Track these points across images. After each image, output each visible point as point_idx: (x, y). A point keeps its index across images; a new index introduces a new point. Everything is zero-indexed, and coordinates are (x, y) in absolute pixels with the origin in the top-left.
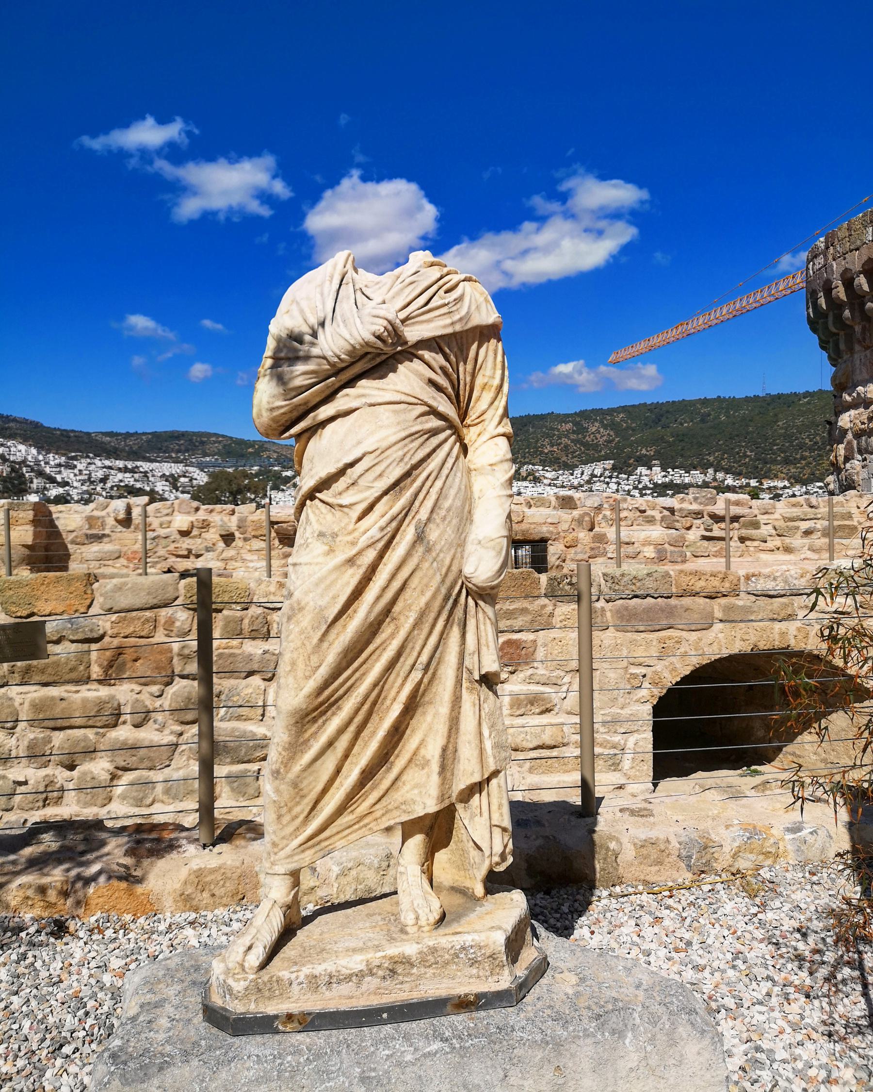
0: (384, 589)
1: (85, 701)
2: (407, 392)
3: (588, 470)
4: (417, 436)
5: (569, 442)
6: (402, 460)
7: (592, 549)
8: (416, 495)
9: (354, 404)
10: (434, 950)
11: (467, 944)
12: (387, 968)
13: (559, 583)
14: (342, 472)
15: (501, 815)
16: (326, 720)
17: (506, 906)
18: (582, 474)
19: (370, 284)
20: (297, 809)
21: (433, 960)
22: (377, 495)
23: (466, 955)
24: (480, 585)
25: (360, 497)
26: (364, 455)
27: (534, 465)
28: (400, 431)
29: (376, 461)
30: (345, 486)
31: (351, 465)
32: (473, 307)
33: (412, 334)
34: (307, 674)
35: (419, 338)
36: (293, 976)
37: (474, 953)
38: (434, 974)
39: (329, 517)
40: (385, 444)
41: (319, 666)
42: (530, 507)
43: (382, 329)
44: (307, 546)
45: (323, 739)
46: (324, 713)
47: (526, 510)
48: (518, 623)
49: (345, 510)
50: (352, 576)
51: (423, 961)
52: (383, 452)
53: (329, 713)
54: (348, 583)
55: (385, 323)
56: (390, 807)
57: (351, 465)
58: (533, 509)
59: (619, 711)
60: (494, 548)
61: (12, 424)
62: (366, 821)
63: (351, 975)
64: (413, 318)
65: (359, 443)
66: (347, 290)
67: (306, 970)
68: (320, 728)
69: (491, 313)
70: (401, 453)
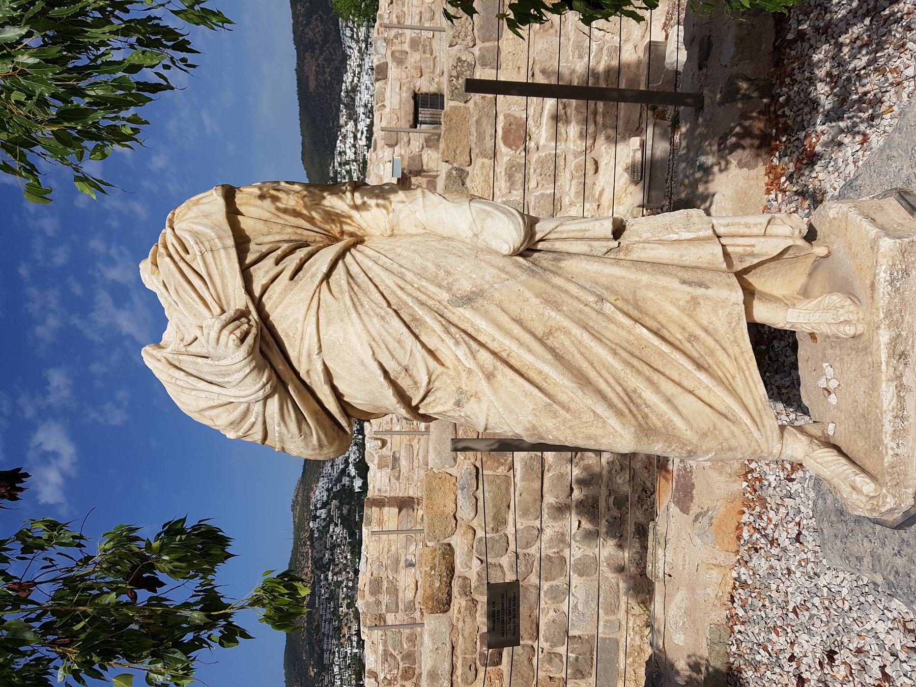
0: (521, 344)
1: (522, 480)
2: (306, 308)
3: (348, 42)
4: (355, 300)
5: (322, 57)
6: (383, 318)
7: (424, 52)
8: (422, 303)
9: (320, 367)
10: (889, 314)
11: (888, 278)
12: (898, 361)
13: (456, 88)
14: (393, 384)
15: (755, 225)
16: (645, 404)
17: (843, 226)
18: (350, 47)
19: (179, 336)
20: (726, 433)
21: (898, 315)
22: (420, 347)
23: (898, 280)
24: (522, 239)
25: (421, 367)
26: (376, 360)
27: (341, 91)
28: (350, 319)
29: (383, 346)
30: (408, 379)
31: (386, 373)
32: (206, 221)
33: (239, 300)
34: (601, 425)
35: (243, 291)
36: (890, 452)
37: (897, 272)
38: (910, 314)
39: (439, 394)
40: (365, 336)
41: (594, 412)
42: (384, 106)
43: (233, 337)
44: (468, 417)
45: (664, 407)
46: (637, 406)
47: (387, 110)
48: (490, 131)
49: (433, 378)
50: (504, 375)
51: (897, 325)
52: (374, 340)
53: (639, 401)
54: (512, 380)
55: (226, 332)
56: (732, 339)
57: (386, 373)
58: (387, 103)
59: (571, 42)
60: (484, 220)
61: (299, 499)
62: (743, 363)
63: (899, 396)
64: (218, 296)
65: (362, 363)
66: (187, 362)
67: (887, 440)
68: (653, 411)
69: (212, 198)
70: (375, 320)
